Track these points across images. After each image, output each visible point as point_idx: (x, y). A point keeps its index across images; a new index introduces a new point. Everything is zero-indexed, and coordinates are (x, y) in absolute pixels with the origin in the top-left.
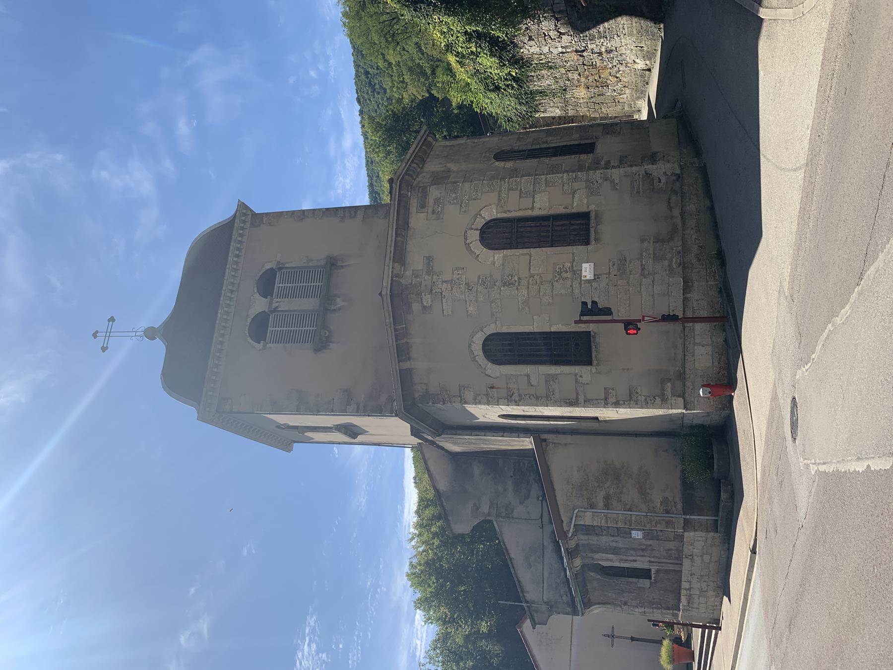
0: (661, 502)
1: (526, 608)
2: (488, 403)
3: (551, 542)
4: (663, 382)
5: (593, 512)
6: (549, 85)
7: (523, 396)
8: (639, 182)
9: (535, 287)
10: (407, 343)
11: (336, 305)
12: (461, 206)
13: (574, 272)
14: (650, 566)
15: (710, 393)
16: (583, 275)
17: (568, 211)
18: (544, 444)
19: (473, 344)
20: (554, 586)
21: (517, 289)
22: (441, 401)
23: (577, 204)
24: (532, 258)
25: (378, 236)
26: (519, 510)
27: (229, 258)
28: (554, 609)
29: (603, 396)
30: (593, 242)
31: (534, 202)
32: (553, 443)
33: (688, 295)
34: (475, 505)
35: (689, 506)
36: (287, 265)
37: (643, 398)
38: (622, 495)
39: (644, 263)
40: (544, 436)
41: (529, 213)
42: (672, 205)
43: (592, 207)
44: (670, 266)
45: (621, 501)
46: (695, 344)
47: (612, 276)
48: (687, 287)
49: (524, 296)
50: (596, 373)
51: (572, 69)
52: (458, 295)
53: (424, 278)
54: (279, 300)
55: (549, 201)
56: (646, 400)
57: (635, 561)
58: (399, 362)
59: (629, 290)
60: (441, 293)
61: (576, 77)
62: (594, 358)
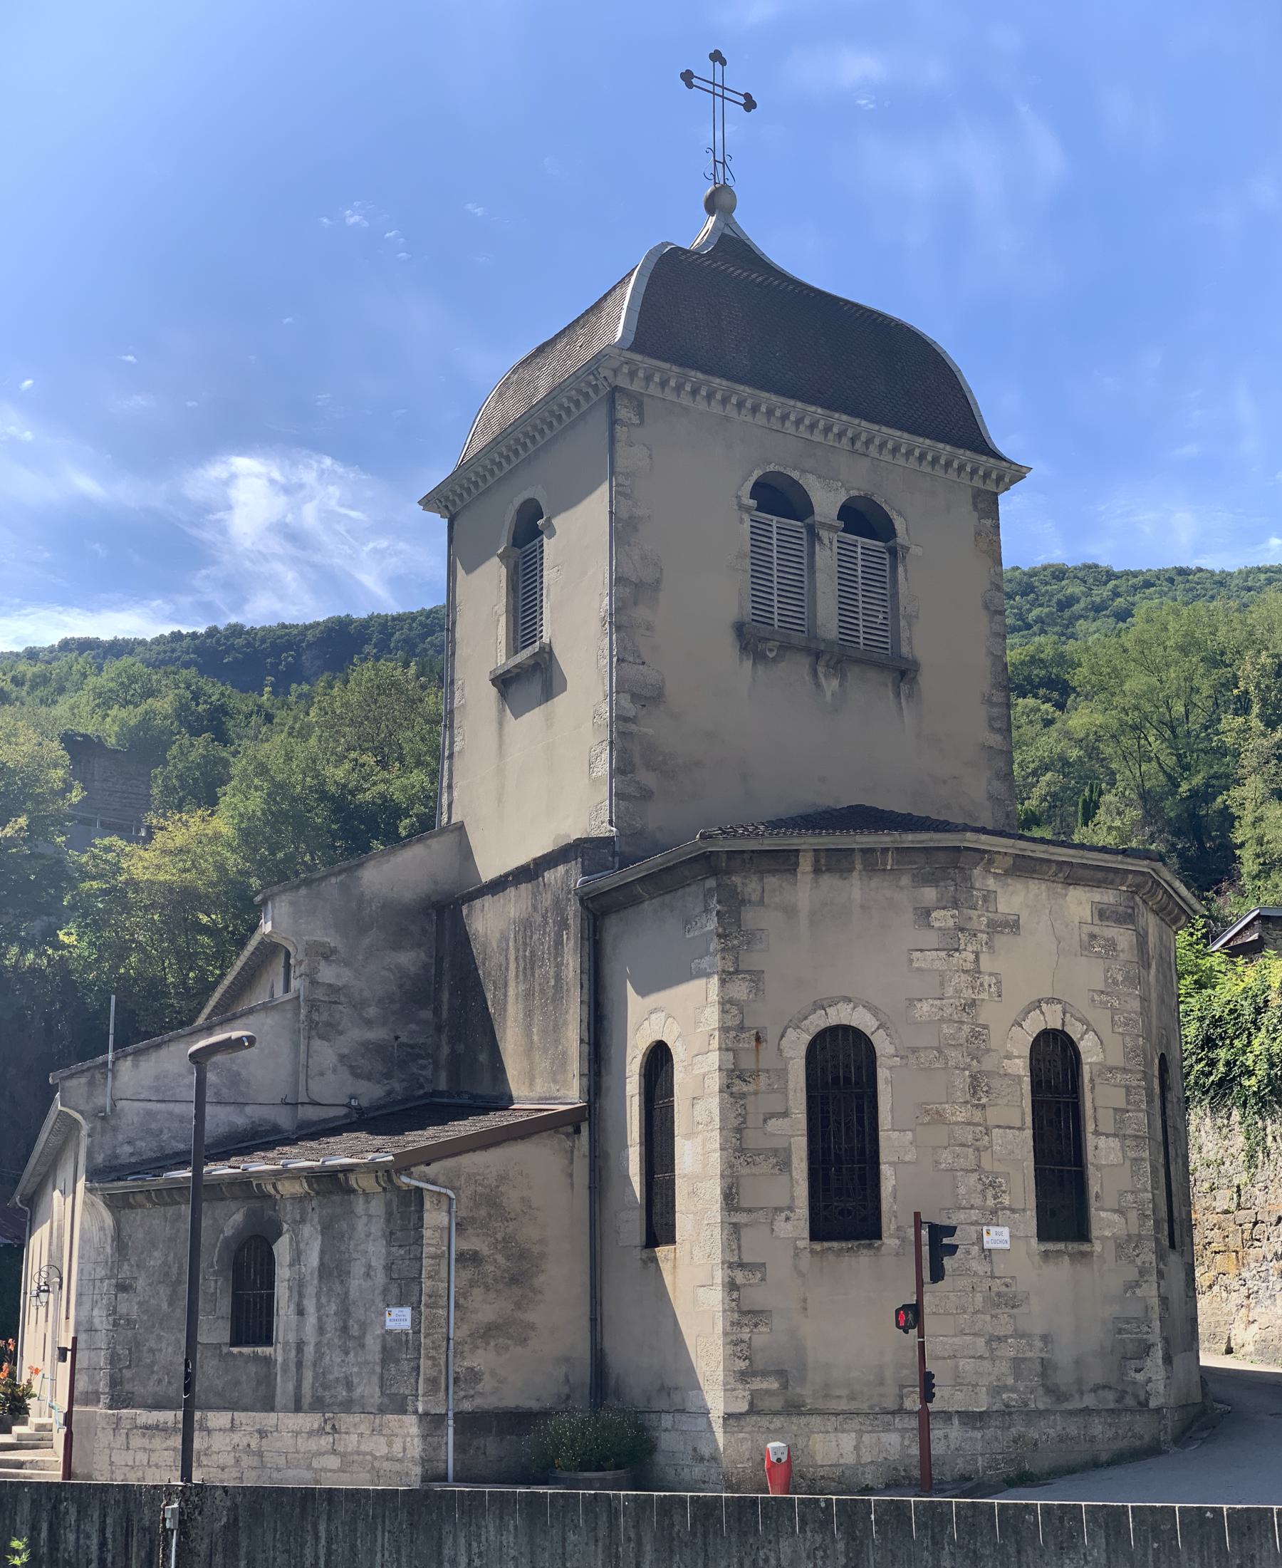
0: (472, 1369)
1: (100, 1059)
2: (724, 1029)
3: (254, 1122)
4: (781, 1374)
5: (449, 1228)
6: (1200, 1148)
7: (742, 1102)
8: (1137, 1333)
9: (970, 1137)
10: (851, 870)
11: (825, 675)
12: (1102, 992)
13: (994, 1212)
14: (286, 1343)
15: (779, 1460)
16: (991, 1228)
17: (1092, 1201)
18: (570, 1129)
19: (851, 1005)
20: (153, 1126)
21: (966, 1102)
22: (725, 929)
23: (1103, 1219)
24: (1017, 1132)
25: (955, 778)
26: (325, 1053)
27: (921, 440)
28: (99, 1124)
29: (747, 1259)
30: (1043, 1247)
31: (1108, 1136)
32: (573, 1147)
33: (956, 1421)
34: (334, 951)
35: (470, 1424)
36: (900, 569)
37: (746, 1337)
38: (482, 1290)
39: (1009, 1341)
40: (585, 1128)
41: (1090, 1127)
42: (1100, 1392)
43: (1097, 1246)
44: (1006, 1388)
45: (471, 1286)
46: (860, 1433)
47: (988, 1282)
48: (971, 1419)
49: (952, 1115)
50: (796, 1248)
51: (1243, 1199)
52: (953, 984)
53: (983, 915)
54: (836, 544)
55: (1108, 1165)
56: (742, 1341)
57: (301, 1312)
58: (815, 850)
59: (965, 1312)
60: (957, 950)
61: (1222, 1204)
62: (826, 1245)
